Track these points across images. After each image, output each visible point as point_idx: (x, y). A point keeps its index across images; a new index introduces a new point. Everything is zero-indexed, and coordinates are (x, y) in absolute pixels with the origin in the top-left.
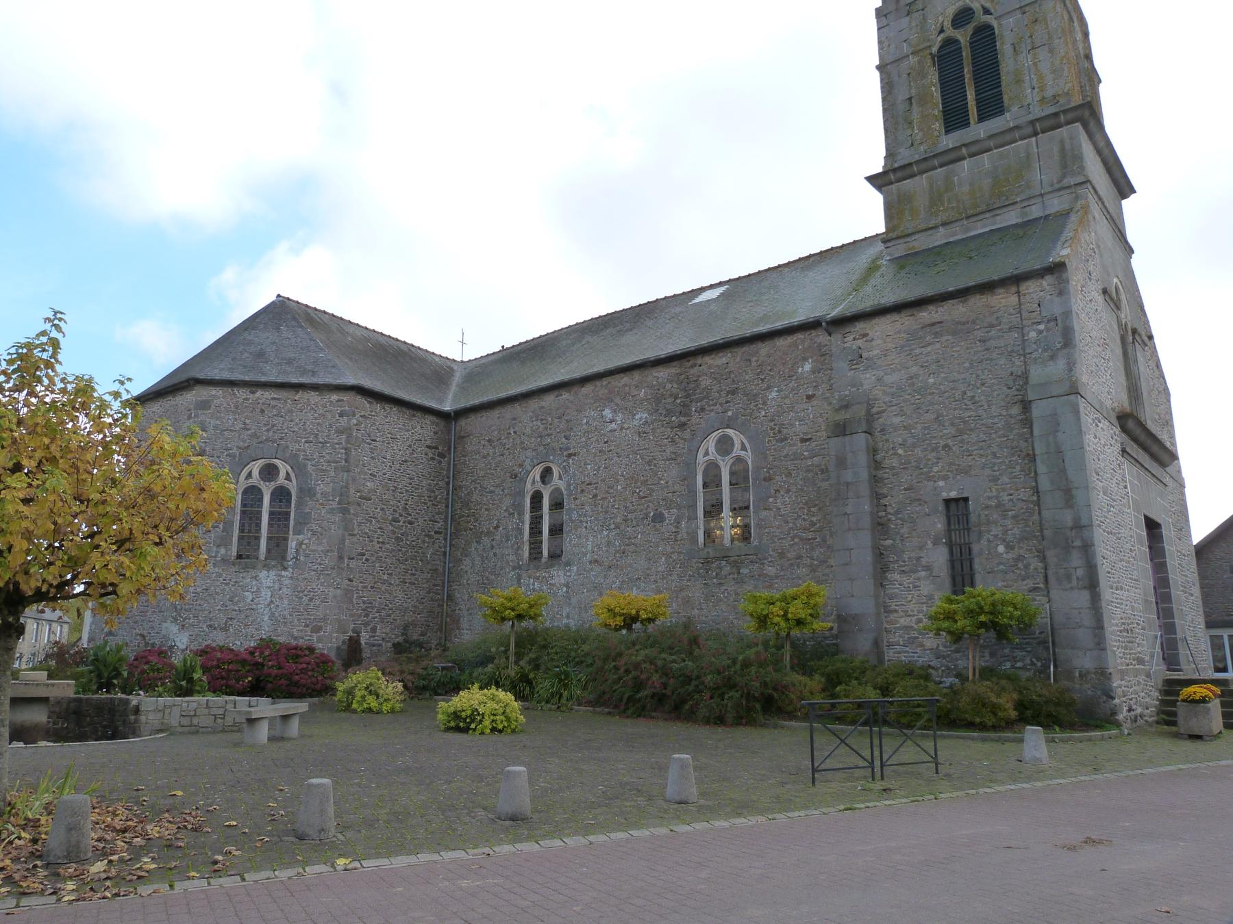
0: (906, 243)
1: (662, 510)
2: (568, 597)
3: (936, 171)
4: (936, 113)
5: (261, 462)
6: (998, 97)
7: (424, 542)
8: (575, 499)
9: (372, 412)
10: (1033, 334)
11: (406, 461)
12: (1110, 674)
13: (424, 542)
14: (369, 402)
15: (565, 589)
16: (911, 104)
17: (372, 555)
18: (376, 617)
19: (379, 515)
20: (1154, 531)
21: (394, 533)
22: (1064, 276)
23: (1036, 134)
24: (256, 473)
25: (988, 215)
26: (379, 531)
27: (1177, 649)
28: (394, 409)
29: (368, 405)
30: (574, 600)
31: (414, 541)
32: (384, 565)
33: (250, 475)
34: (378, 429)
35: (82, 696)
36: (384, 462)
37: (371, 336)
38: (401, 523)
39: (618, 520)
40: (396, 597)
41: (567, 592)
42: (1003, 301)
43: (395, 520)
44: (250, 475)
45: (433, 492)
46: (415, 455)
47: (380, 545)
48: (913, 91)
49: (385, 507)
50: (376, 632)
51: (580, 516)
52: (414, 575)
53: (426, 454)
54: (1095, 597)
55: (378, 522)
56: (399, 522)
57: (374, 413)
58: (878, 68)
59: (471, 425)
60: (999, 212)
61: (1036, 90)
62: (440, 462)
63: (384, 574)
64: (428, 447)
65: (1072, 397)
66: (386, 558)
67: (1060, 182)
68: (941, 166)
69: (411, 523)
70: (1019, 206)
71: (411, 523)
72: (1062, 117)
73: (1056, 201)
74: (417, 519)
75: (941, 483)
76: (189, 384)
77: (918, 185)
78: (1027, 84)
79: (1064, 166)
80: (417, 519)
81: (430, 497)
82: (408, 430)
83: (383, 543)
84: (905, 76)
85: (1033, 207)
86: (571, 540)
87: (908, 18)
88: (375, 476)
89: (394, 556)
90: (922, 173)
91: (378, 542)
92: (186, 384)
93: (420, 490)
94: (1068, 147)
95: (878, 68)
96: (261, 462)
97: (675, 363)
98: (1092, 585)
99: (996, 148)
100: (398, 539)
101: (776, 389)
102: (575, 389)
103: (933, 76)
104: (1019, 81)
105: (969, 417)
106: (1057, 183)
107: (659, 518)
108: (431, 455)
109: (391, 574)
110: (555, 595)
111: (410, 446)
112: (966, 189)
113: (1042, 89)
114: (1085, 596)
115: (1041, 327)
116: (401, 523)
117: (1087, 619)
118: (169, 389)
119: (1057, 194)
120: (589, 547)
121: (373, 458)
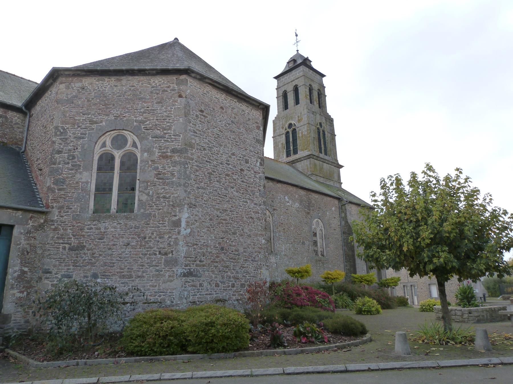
1: (304, 240)
2: (277, 268)
5: (114, 134)
6: (323, 151)
8: (277, 228)
15: (276, 265)
24: (108, 143)
30: (279, 270)
33: (104, 145)
35: (344, 343)
39: (292, 241)
41: (276, 266)
44: (104, 145)
51: (279, 235)
68: (322, 162)
76: (258, 106)
86: (277, 245)
90: (319, 160)
92: (258, 104)
96: (114, 134)
97: (305, 191)
102: (275, 183)
107: (303, 243)
110: (272, 266)
118: (234, 93)
120: (283, 249)
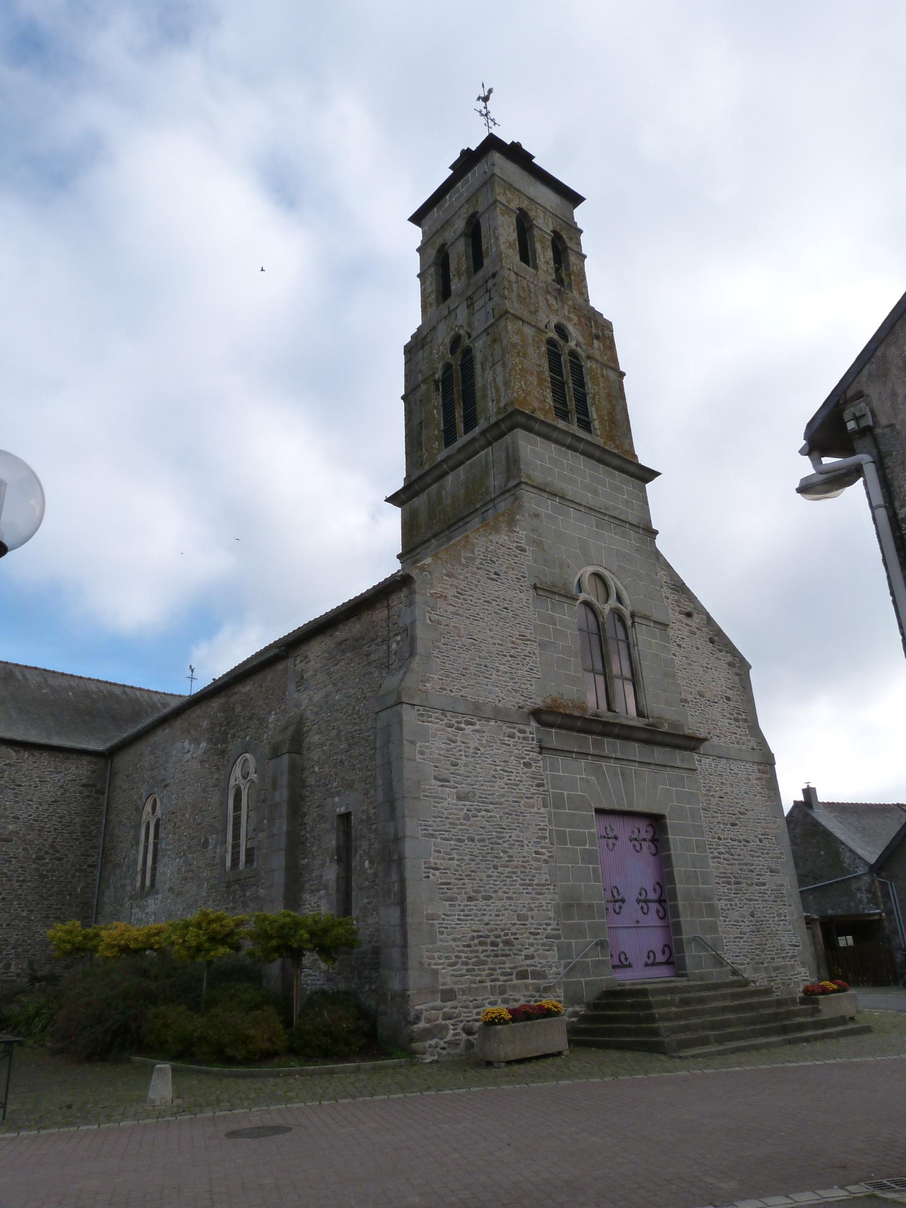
0: (413, 556)
3: (433, 487)
4: (436, 433)
7: (74, 876)
9: (18, 759)
10: (394, 646)
11: (55, 801)
12: (409, 996)
13: (74, 876)
14: (15, 751)
16: (421, 427)
17: (10, 894)
18: (11, 954)
19: (21, 855)
20: (662, 821)
21: (37, 870)
22: (413, 589)
23: (490, 444)
25: (461, 524)
26: (20, 870)
27: (683, 952)
28: (45, 754)
29: (14, 754)
31: (61, 877)
32: (24, 903)
34: (24, 775)
36: (29, 805)
37: (72, 684)
38: (47, 861)
40: (37, 932)
42: (380, 615)
43: (40, 858)
45: (88, 827)
46: (68, 795)
47: (20, 883)
48: (423, 415)
49: (28, 847)
50: (10, 969)
52: (60, 909)
53: (81, 793)
54: (403, 913)
55: (20, 861)
56: (45, 859)
57: (20, 761)
58: (403, 398)
59: (124, 761)
60: (468, 519)
61: (495, 402)
62: (97, 799)
63: (23, 911)
64: (84, 786)
65: (398, 707)
66: (26, 896)
67: (506, 485)
69: (59, 859)
70: (479, 512)
71: (59, 859)
72: (503, 426)
73: (503, 504)
74: (66, 855)
75: (337, 799)
77: (420, 501)
78: (489, 399)
79: (508, 470)
80: (66, 855)
81: (83, 833)
82: (60, 772)
83: (24, 881)
84: (418, 402)
85: (490, 511)
87: (422, 351)
88: (18, 818)
89: (36, 893)
91: (18, 881)
93: (72, 828)
94: (511, 451)
95: (403, 398)
98: (402, 902)
99: (467, 460)
100: (42, 876)
101: (274, 712)
103: (437, 400)
104: (485, 396)
105: (355, 731)
106: (504, 486)
108: (86, 793)
109: (32, 911)
111: (62, 787)
112: (449, 501)
113: (498, 401)
114: (395, 912)
115: (399, 638)
116: (47, 861)
117: (398, 941)
119: (503, 498)
121: (17, 802)
